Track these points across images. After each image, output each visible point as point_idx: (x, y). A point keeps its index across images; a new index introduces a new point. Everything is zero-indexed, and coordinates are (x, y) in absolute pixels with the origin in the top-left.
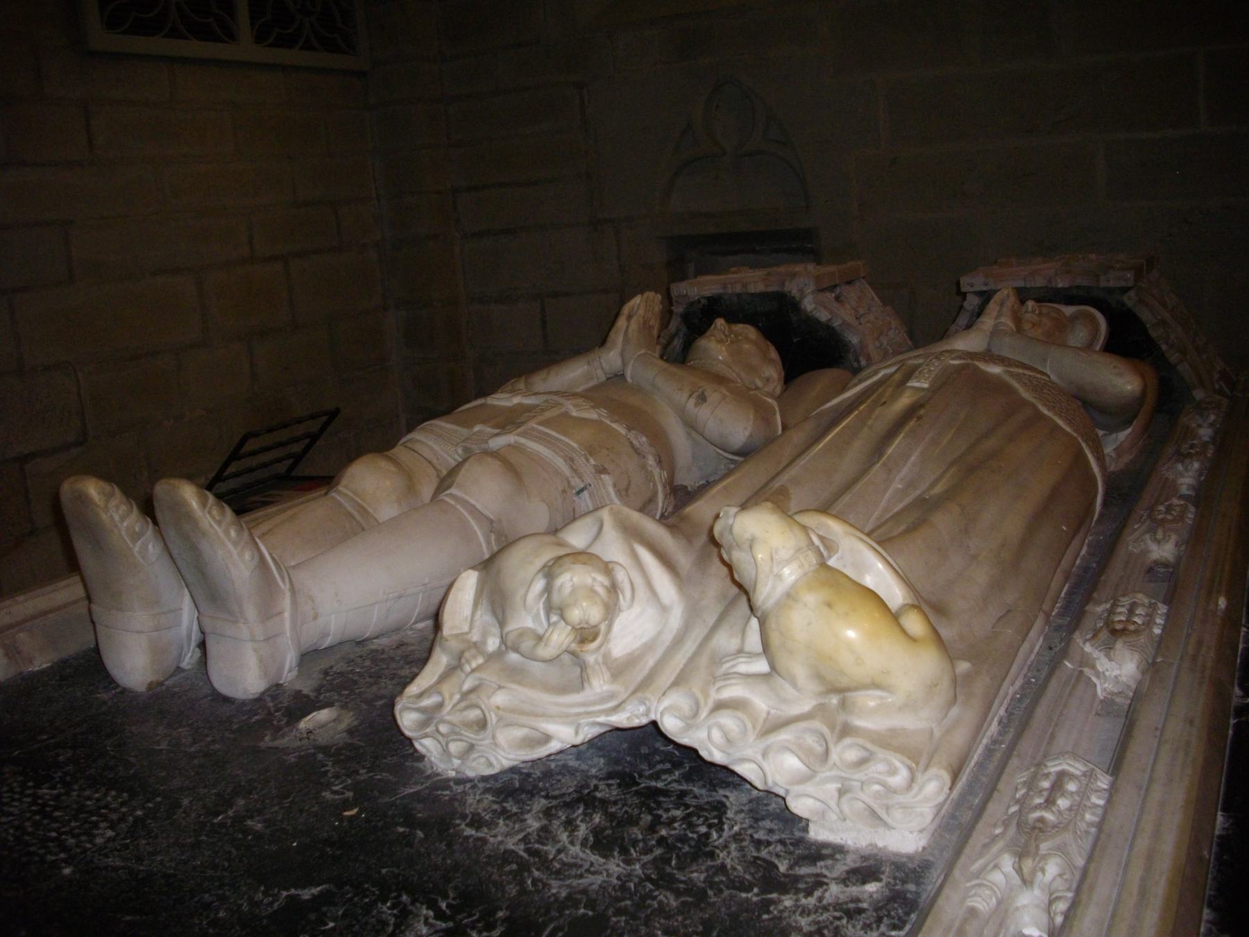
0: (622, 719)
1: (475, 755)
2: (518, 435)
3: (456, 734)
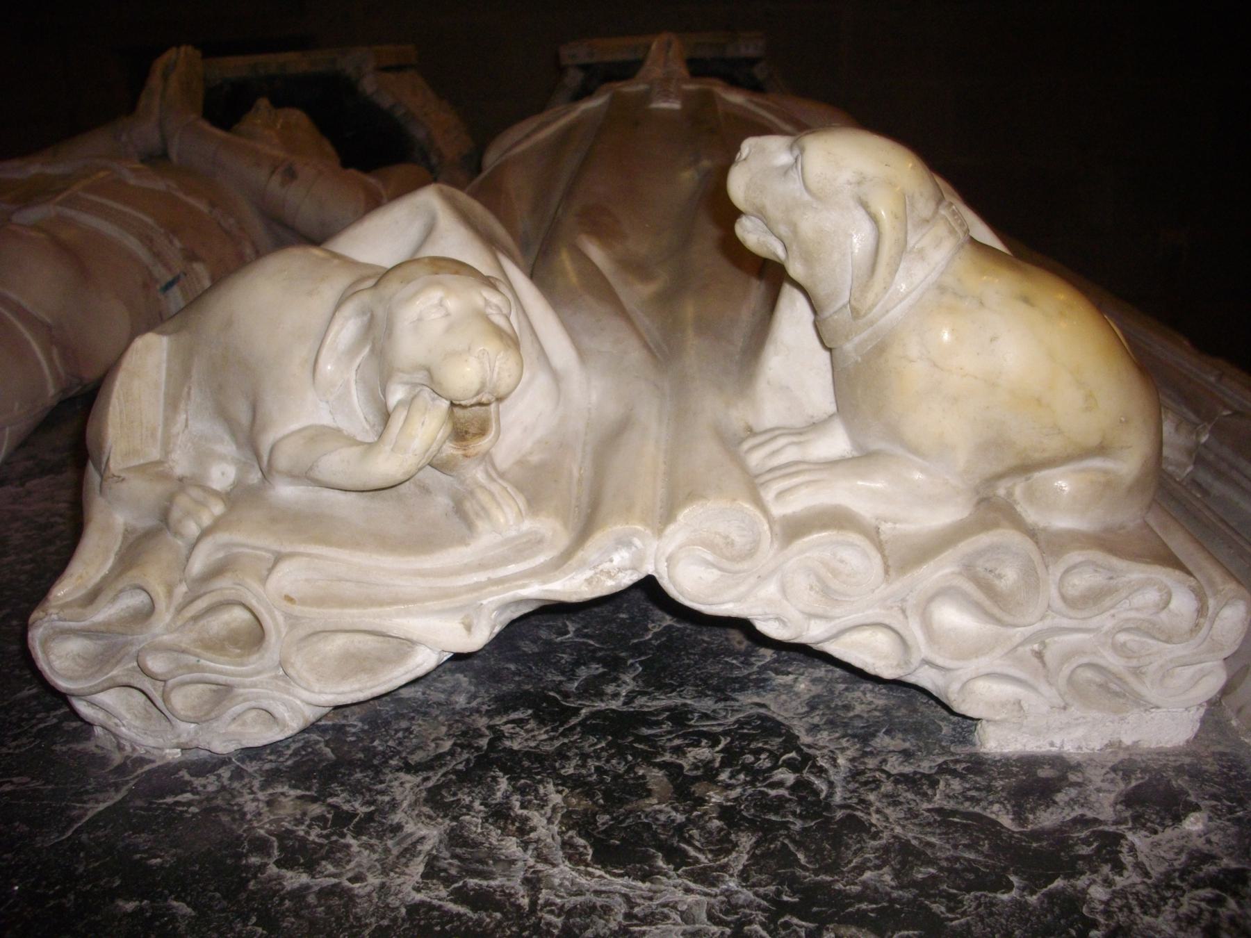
0: (573, 585)
1: (238, 709)
2: (60, 204)
3: (190, 669)
